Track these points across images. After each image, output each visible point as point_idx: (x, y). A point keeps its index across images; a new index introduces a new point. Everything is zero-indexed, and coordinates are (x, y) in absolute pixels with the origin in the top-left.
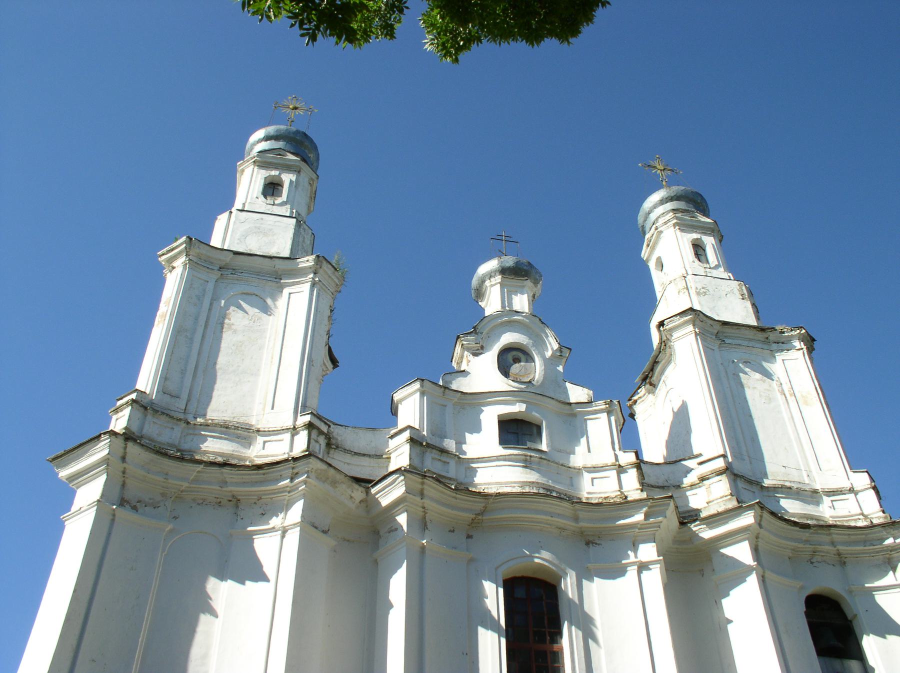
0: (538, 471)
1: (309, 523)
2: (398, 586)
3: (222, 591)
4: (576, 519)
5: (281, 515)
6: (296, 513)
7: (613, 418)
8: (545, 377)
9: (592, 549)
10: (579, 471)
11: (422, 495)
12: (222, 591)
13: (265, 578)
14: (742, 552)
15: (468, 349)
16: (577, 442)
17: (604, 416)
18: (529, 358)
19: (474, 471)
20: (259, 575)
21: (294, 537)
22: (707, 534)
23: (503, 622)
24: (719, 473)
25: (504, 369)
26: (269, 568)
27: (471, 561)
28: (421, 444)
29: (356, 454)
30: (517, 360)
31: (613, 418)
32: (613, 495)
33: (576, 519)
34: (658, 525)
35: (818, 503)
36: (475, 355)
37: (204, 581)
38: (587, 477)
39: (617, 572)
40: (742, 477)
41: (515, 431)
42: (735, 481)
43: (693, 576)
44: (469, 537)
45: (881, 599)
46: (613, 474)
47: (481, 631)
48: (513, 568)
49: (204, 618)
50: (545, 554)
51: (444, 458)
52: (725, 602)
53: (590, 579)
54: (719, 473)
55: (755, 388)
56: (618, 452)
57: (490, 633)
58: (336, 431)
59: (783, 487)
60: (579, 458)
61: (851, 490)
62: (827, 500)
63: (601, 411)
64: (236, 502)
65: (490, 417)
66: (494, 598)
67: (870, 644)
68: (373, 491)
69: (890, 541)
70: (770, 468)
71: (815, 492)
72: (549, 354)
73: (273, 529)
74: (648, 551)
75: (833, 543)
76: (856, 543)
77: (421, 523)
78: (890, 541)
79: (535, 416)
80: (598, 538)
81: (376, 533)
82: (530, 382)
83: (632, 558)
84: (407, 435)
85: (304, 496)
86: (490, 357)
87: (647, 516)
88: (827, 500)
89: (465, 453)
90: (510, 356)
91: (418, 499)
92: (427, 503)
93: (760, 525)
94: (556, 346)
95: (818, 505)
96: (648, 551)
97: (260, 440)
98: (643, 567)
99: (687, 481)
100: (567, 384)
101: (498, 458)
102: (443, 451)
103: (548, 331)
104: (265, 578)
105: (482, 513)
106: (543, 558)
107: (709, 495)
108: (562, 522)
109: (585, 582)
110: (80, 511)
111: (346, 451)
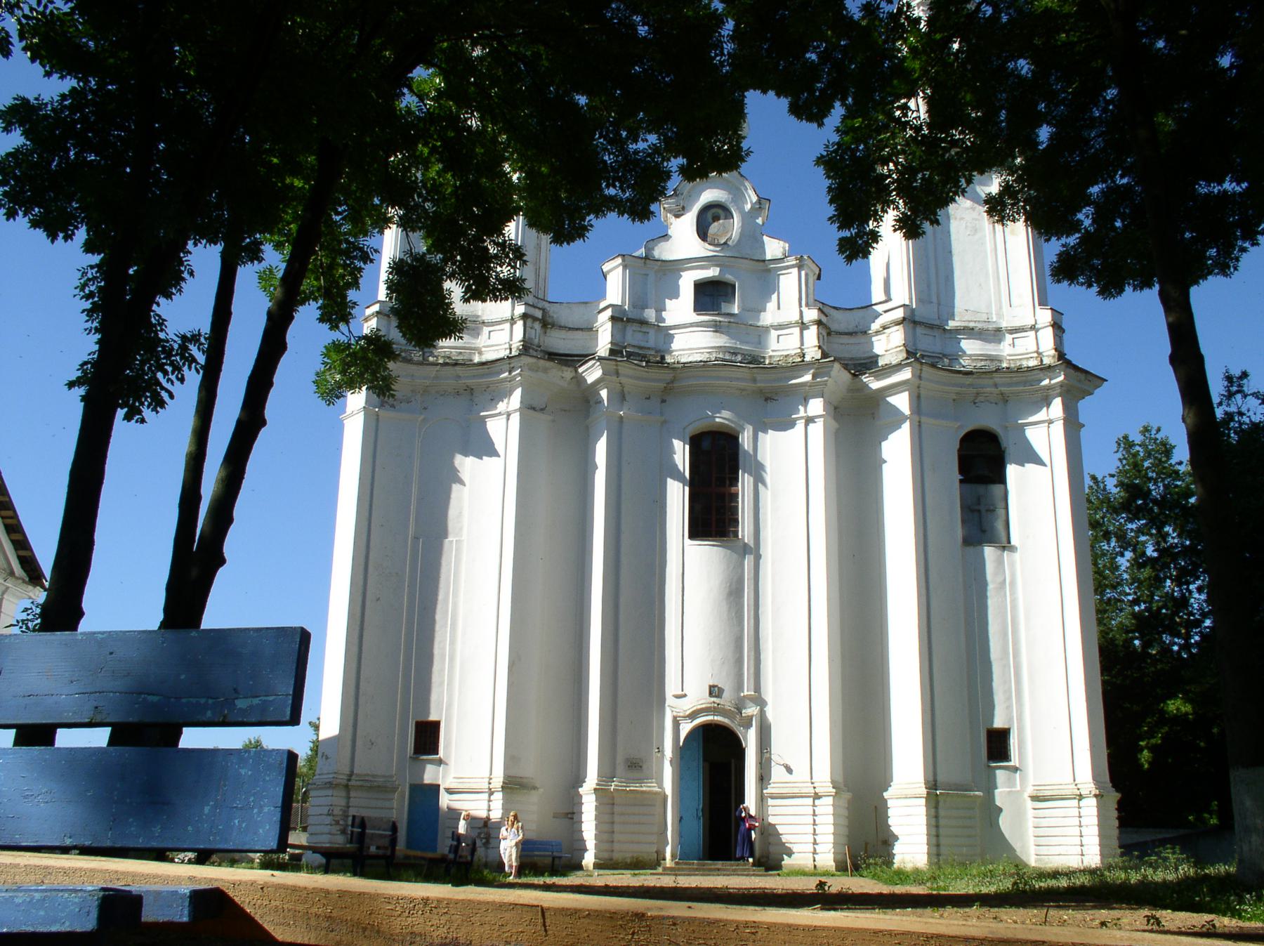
0: (727, 334)
1: (528, 408)
2: (601, 448)
3: (466, 465)
4: (754, 380)
5: (506, 401)
6: (516, 399)
7: (803, 273)
8: (742, 234)
9: (770, 404)
10: (766, 329)
11: (617, 374)
12: (466, 465)
13: (496, 454)
14: (901, 401)
15: (670, 211)
16: (768, 299)
17: (795, 270)
18: (729, 215)
19: (672, 336)
20: (493, 452)
21: (516, 418)
22: (875, 385)
23: (687, 474)
24: (897, 323)
25: (702, 233)
26: (499, 446)
27: (665, 422)
28: (622, 320)
29: (570, 329)
30: (716, 218)
31: (803, 273)
32: (793, 352)
33: (754, 380)
34: (825, 383)
35: (999, 341)
36: (677, 216)
37: (452, 458)
38: (774, 334)
39: (788, 425)
40: (920, 323)
41: (710, 295)
42: (914, 329)
43: (857, 423)
44: (663, 401)
45: (1030, 433)
46: (797, 330)
47: (669, 480)
48: (698, 427)
49: (456, 487)
50: (726, 414)
51: (645, 329)
52: (884, 444)
53: (765, 431)
54: (897, 323)
55: (962, 219)
56: (804, 309)
57: (676, 483)
58: (552, 309)
59: (965, 328)
60: (769, 317)
61: (1033, 328)
62: (1009, 337)
63: (792, 266)
64: (470, 390)
65: (687, 281)
66: (681, 454)
67: (1012, 471)
68: (580, 370)
69: (1046, 382)
70: (960, 303)
71: (999, 330)
72: (748, 207)
73: (500, 414)
74: (816, 406)
75: (996, 386)
76: (1017, 384)
77: (620, 396)
78: (1046, 382)
79: (729, 277)
80: (772, 395)
81: (587, 401)
82: (725, 243)
83: (802, 413)
84: (609, 312)
85: (521, 385)
86: (690, 219)
87: (814, 377)
88: (1009, 337)
89: (664, 321)
90: (709, 215)
91: (614, 378)
92: (623, 380)
93: (920, 378)
94: (755, 199)
95: (692, 536)
96: (816, 406)
97: (486, 330)
98: (809, 420)
99: (875, 326)
100: (765, 238)
101: (691, 325)
102: (643, 322)
103: (747, 184)
104: (496, 454)
105: (672, 382)
106: (723, 418)
107: (888, 344)
108: (743, 385)
109: (760, 434)
110: (352, 414)
111: (561, 327)
